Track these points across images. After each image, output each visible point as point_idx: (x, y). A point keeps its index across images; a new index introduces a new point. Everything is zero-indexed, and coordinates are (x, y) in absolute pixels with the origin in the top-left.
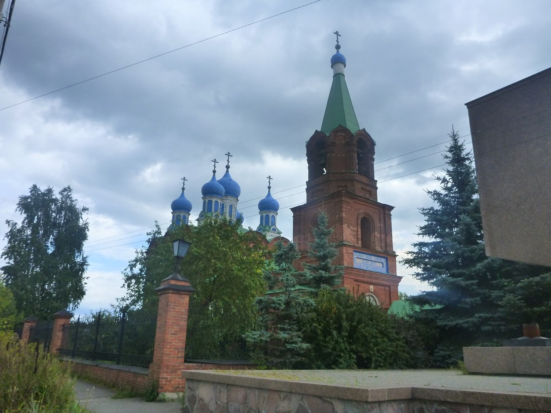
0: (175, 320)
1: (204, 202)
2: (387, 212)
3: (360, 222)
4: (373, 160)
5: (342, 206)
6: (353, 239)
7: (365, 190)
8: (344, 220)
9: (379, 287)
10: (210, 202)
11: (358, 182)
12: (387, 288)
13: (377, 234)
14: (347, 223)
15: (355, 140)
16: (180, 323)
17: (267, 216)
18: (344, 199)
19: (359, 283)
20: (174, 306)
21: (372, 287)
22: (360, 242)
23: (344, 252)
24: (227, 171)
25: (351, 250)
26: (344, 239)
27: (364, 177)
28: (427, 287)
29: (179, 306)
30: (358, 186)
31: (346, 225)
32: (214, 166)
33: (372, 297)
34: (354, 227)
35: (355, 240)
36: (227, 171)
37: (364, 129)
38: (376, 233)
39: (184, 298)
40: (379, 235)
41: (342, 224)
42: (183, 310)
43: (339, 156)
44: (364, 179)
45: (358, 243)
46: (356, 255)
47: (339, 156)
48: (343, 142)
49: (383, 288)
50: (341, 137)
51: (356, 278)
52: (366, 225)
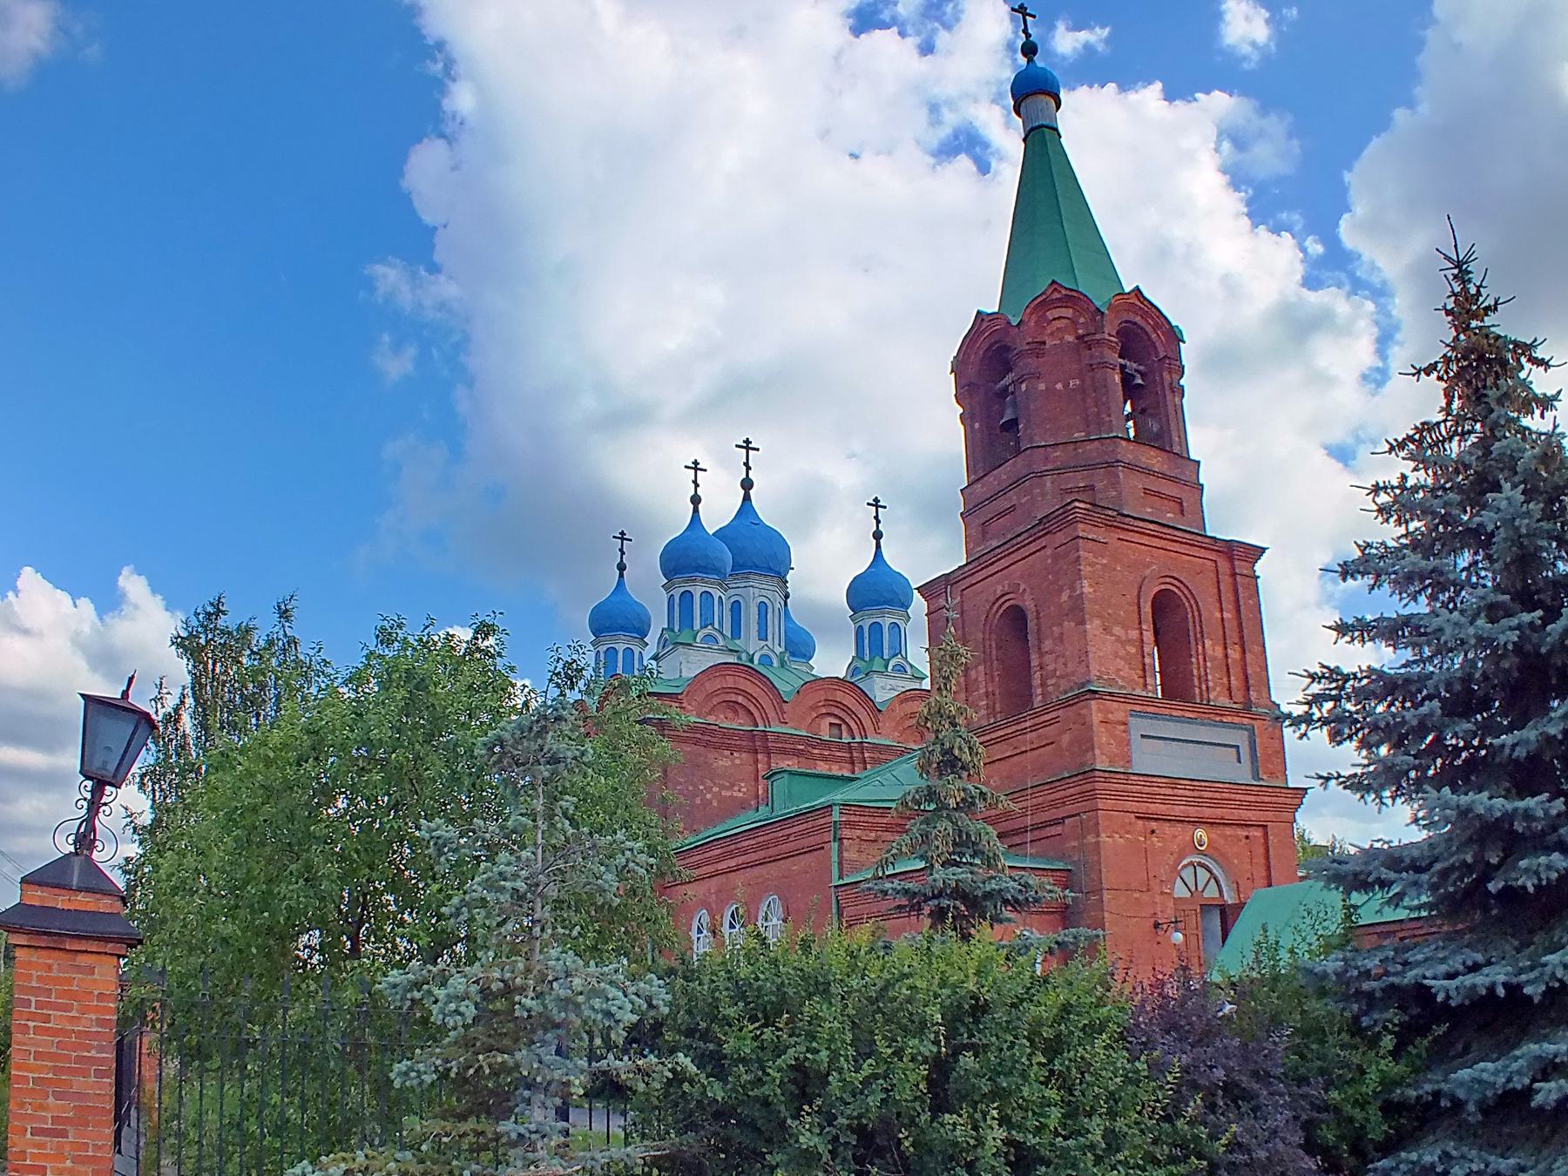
0: (56, 1070)
2: (1241, 567)
3: (1147, 609)
7: (1157, 494)
8: (1087, 605)
9: (1228, 831)
10: (687, 596)
11: (1131, 467)
12: (1258, 833)
13: (1212, 648)
14: (1100, 616)
15: (1110, 330)
16: (78, 1084)
17: (876, 627)
18: (1081, 529)
19: (1154, 825)
20: (39, 1005)
21: (1200, 833)
23: (1096, 718)
24: (747, 498)
25: (1119, 711)
26: (1094, 672)
27: (1153, 452)
28: (1398, 824)
29: (68, 1008)
30: (1132, 484)
31: (1097, 622)
32: (695, 482)
33: (1200, 864)
34: (1126, 628)
35: (1135, 675)
36: (747, 498)
37: (1137, 290)
38: (1208, 643)
39: (91, 970)
40: (1219, 652)
41: (1083, 622)
42: (89, 1023)
44: (1153, 459)
46: (1139, 726)
47: (1059, 386)
48: (1070, 338)
49: (1242, 833)
51: (1143, 808)
52: (1168, 617)
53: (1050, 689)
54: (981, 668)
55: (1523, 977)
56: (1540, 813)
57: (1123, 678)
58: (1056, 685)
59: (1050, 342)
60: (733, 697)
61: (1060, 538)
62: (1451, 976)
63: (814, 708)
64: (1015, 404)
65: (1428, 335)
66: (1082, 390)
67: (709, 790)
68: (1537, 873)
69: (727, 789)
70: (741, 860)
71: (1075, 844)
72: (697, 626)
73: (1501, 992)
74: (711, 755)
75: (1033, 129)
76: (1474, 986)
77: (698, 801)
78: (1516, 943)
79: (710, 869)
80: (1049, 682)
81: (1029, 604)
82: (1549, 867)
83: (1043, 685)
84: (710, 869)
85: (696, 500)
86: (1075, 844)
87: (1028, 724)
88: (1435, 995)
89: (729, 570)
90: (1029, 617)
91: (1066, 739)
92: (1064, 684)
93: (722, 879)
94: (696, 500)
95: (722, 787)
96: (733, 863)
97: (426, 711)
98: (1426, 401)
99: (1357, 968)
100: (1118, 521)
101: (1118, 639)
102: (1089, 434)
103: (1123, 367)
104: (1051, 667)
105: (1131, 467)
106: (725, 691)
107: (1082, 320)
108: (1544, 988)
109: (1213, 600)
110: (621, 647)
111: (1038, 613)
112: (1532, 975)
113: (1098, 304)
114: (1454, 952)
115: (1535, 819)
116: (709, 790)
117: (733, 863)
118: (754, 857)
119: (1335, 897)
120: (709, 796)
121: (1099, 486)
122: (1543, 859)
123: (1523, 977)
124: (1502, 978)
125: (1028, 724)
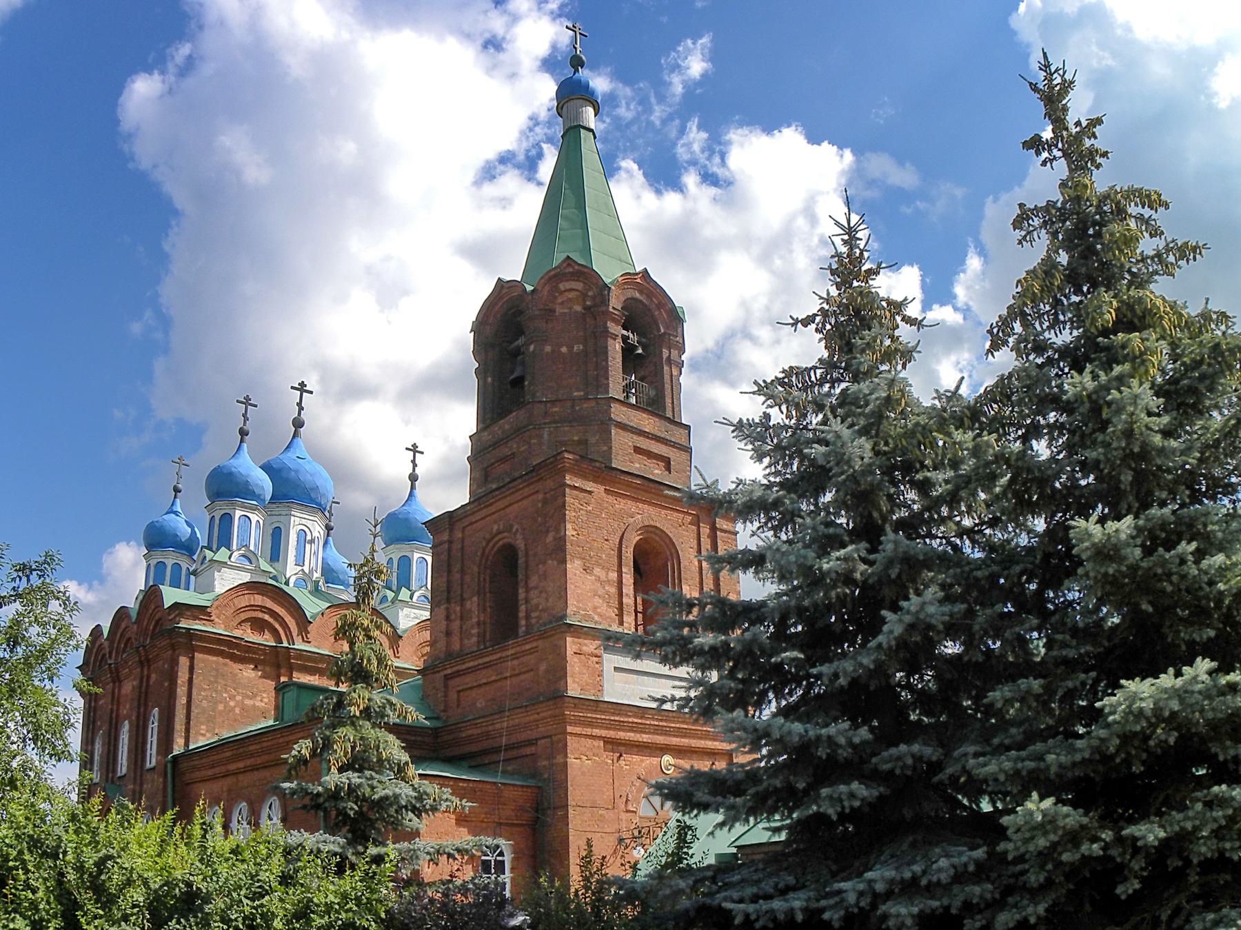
1: (148, 567)
3: (628, 554)
4: (122, 613)
5: (564, 503)
6: (603, 609)
8: (568, 546)
11: (623, 427)
22: (629, 619)
25: (591, 646)
30: (621, 443)
31: (578, 563)
35: (612, 613)
43: (564, 349)
45: (621, 623)
46: (611, 660)
47: (564, 349)
48: (578, 308)
50: (571, 295)
51: (611, 734)
53: (533, 621)
54: (475, 599)
55: (823, 903)
56: (842, 741)
57: (600, 615)
58: (539, 618)
59: (559, 310)
60: (260, 615)
61: (550, 484)
62: (755, 899)
64: (523, 363)
65: (813, 291)
66: (585, 353)
67: (232, 698)
68: (841, 801)
70: (249, 762)
71: (545, 763)
72: (235, 547)
73: (799, 917)
74: (236, 667)
75: (571, 128)
76: (791, 912)
77: (221, 707)
78: (834, 868)
79: (223, 769)
80: (533, 615)
81: (520, 544)
82: (852, 795)
83: (528, 617)
84: (223, 769)
86: (545, 763)
87: (510, 652)
88: (734, 919)
89: (268, 497)
90: (520, 554)
91: (543, 667)
92: (545, 616)
93: (229, 781)
94: (298, 424)
96: (241, 765)
98: (809, 349)
99: (671, 886)
100: (606, 474)
101: (598, 579)
102: (587, 394)
103: (625, 339)
104: (535, 602)
105: (623, 427)
106: (252, 607)
107: (590, 293)
108: (842, 913)
109: (693, 552)
110: (169, 563)
111: (526, 549)
112: (832, 902)
113: (607, 281)
114: (770, 875)
115: (839, 746)
116: (232, 698)
117: (241, 765)
118: (259, 760)
119: (674, 816)
120: (232, 704)
121: (592, 440)
122: (843, 788)
123: (823, 903)
124: (797, 904)
125: (510, 652)
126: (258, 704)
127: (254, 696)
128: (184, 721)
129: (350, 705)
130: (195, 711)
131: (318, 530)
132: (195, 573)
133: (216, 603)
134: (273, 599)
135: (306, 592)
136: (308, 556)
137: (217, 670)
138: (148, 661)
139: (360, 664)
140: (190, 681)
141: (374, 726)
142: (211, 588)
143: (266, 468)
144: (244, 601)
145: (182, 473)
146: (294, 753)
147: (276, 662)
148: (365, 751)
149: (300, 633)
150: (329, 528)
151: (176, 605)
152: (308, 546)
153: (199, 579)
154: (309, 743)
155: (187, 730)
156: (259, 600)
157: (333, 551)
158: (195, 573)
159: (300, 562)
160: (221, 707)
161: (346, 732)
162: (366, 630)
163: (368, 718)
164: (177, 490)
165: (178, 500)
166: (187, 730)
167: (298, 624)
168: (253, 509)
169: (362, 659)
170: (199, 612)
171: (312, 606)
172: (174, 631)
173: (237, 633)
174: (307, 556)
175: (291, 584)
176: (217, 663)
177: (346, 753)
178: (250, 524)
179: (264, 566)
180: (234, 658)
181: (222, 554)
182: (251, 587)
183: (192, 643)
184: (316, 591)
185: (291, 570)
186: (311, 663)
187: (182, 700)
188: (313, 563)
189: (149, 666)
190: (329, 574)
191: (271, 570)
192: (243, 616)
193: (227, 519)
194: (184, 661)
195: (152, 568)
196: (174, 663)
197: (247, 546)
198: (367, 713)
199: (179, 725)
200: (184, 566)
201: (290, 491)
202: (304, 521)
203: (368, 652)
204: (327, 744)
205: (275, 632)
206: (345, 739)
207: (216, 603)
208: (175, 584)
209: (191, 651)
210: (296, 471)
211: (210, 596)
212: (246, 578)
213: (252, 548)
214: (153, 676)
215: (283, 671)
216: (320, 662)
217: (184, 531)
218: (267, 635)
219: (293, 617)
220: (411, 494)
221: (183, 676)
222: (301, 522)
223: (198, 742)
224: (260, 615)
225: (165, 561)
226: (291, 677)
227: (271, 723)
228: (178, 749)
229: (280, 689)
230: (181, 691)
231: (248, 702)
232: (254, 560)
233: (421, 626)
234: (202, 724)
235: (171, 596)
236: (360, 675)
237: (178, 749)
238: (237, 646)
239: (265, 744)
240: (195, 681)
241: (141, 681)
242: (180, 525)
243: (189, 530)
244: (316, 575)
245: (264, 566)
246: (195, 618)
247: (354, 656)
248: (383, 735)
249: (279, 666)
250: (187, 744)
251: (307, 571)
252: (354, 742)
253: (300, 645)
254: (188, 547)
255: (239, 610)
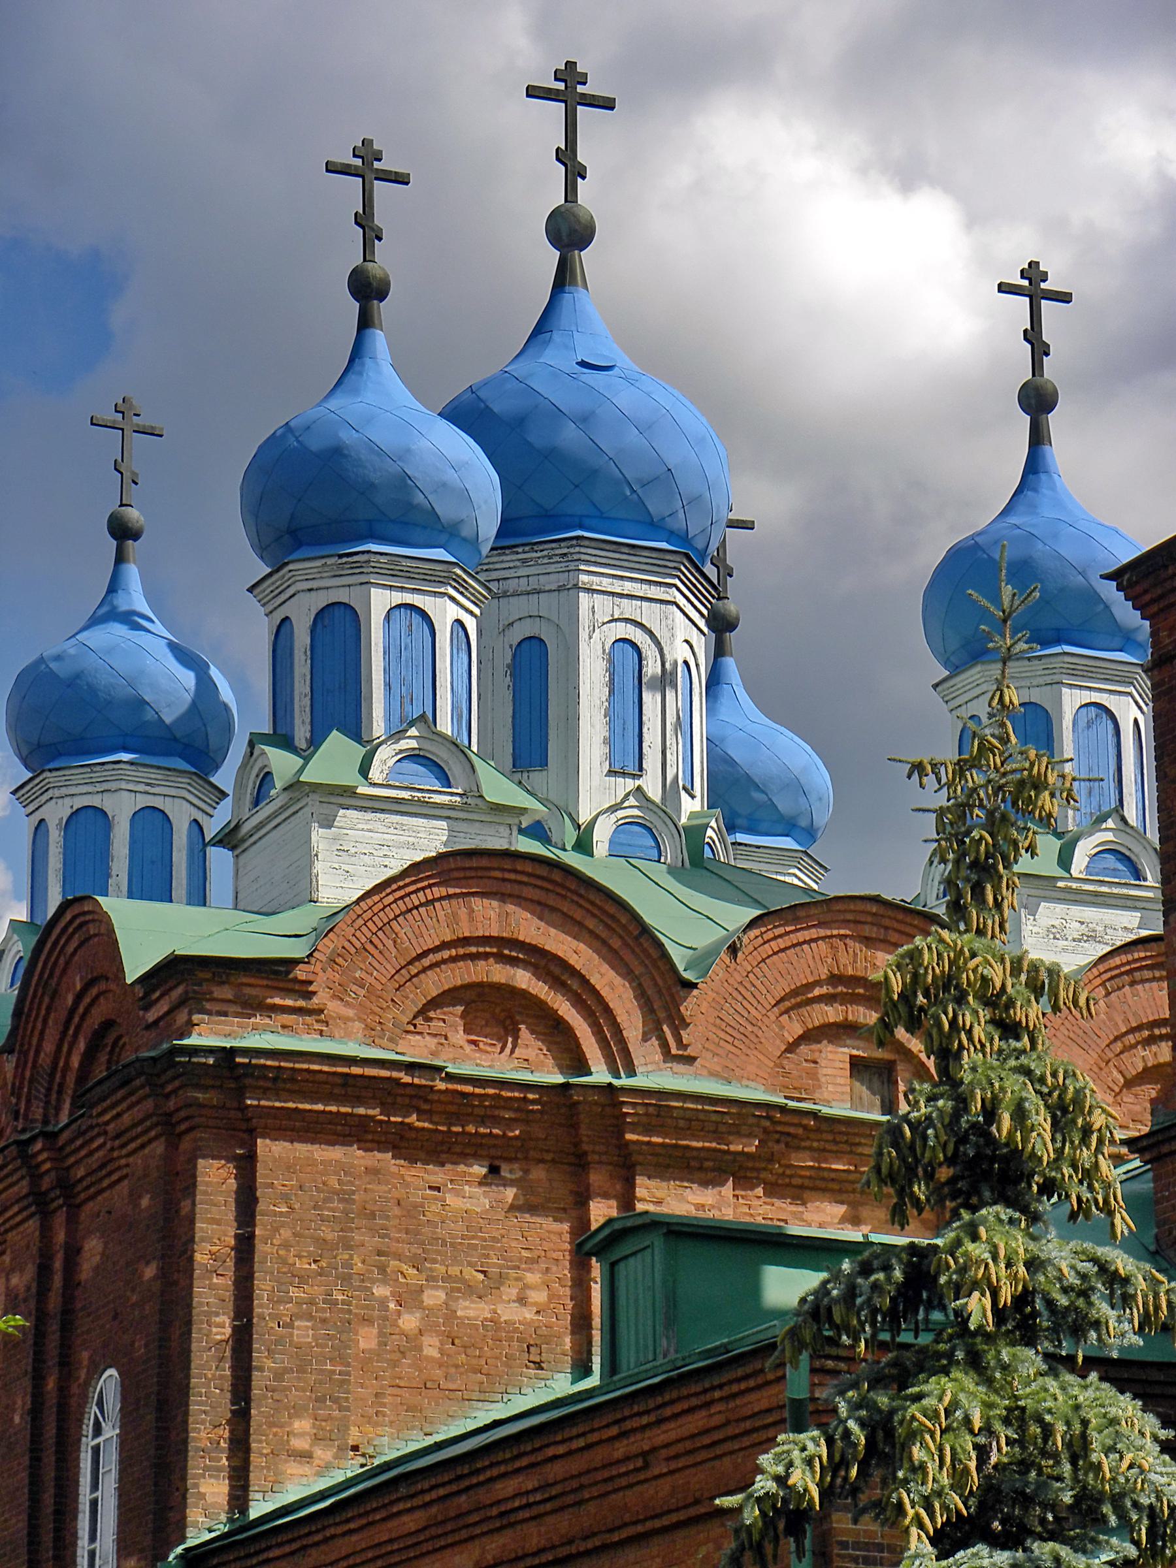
60: (498, 973)
63: (797, 998)
69: (470, 1290)
72: (379, 728)
74: (419, 1177)
85: (570, 233)
89: (488, 526)
94: (570, 233)
95: (461, 1288)
97: (919, 1028)
106: (467, 947)
110: (122, 807)
116: (409, 1298)
120: (409, 1321)
126: (510, 1312)
127: (494, 1283)
128: (225, 1406)
129: (959, 1290)
130: (266, 1364)
131: (683, 637)
132: (230, 838)
133: (328, 946)
134: (542, 909)
135: (658, 871)
136: (644, 725)
137: (345, 1197)
138: (66, 1186)
139: (982, 1131)
140: (245, 1248)
141: (1056, 1363)
142: (302, 892)
143: (468, 414)
144: (439, 923)
145: (135, 464)
146: (763, 1485)
147: (569, 1144)
148: (1025, 1465)
149: (653, 1029)
150: (721, 625)
151: (174, 969)
152: (651, 701)
153: (255, 857)
154: (813, 1442)
155: (240, 1445)
156: (489, 916)
157: (743, 711)
158: (230, 838)
159: (627, 761)
160: (366, 1339)
161: (952, 1391)
162: (996, 1001)
163: (1028, 1335)
164: (123, 531)
165: (132, 571)
166: (240, 1445)
167: (641, 995)
168: (435, 578)
169: (991, 1113)
170: (263, 981)
171: (688, 923)
172: (175, 1066)
173: (416, 1049)
174: (652, 737)
175: (601, 848)
176: (343, 1168)
177: (959, 1476)
178: (429, 633)
179: (497, 787)
180: (405, 1145)
181: (334, 760)
182: (453, 870)
183: (243, 1103)
184: (696, 864)
185: (596, 793)
186: (705, 1139)
187: (214, 1326)
188: (675, 761)
189: (74, 1210)
190: (738, 793)
191: (521, 799)
192: (434, 983)
193: (340, 627)
194: (215, 1177)
195: (55, 837)
196: (178, 1187)
197: (427, 720)
198: (1021, 1318)
199: (207, 1426)
200: (181, 815)
201: (571, 494)
202: (629, 608)
203: (1014, 1085)
204: (887, 1444)
205: (556, 1033)
206: (953, 1421)
207: (328, 946)
208: (152, 884)
209: (240, 1140)
210: (584, 420)
211: (301, 919)
212: (429, 838)
213: (445, 725)
214: (93, 1247)
215: (596, 1178)
216: (736, 1131)
217: (170, 687)
218: (530, 1045)
219: (627, 973)
220: (1035, 465)
221: (213, 1234)
222: (618, 613)
223: (291, 1483)
224: (498, 973)
225: (107, 803)
226: (627, 1201)
227: (562, 1385)
228: (204, 1523)
229: (587, 1247)
230: (211, 1297)
231: (471, 1310)
232: (455, 769)
233: (1122, 964)
234: (297, 1412)
235: (146, 934)
236: (988, 1171)
237: (204, 1523)
238: (419, 1099)
239: (556, 1470)
240: (262, 1248)
241: (44, 1271)
242: (148, 664)
243: (188, 678)
244: (691, 806)
245: (497, 787)
246: (252, 1007)
247: (962, 1103)
248: (1096, 1396)
249: (579, 1163)
250: (239, 1498)
251: (654, 791)
252: (988, 1429)
253: (653, 1074)
254: (190, 745)
255: (420, 961)
